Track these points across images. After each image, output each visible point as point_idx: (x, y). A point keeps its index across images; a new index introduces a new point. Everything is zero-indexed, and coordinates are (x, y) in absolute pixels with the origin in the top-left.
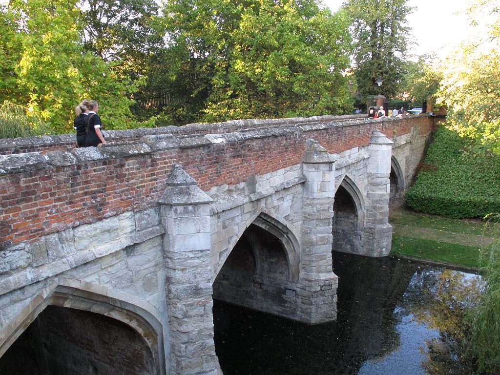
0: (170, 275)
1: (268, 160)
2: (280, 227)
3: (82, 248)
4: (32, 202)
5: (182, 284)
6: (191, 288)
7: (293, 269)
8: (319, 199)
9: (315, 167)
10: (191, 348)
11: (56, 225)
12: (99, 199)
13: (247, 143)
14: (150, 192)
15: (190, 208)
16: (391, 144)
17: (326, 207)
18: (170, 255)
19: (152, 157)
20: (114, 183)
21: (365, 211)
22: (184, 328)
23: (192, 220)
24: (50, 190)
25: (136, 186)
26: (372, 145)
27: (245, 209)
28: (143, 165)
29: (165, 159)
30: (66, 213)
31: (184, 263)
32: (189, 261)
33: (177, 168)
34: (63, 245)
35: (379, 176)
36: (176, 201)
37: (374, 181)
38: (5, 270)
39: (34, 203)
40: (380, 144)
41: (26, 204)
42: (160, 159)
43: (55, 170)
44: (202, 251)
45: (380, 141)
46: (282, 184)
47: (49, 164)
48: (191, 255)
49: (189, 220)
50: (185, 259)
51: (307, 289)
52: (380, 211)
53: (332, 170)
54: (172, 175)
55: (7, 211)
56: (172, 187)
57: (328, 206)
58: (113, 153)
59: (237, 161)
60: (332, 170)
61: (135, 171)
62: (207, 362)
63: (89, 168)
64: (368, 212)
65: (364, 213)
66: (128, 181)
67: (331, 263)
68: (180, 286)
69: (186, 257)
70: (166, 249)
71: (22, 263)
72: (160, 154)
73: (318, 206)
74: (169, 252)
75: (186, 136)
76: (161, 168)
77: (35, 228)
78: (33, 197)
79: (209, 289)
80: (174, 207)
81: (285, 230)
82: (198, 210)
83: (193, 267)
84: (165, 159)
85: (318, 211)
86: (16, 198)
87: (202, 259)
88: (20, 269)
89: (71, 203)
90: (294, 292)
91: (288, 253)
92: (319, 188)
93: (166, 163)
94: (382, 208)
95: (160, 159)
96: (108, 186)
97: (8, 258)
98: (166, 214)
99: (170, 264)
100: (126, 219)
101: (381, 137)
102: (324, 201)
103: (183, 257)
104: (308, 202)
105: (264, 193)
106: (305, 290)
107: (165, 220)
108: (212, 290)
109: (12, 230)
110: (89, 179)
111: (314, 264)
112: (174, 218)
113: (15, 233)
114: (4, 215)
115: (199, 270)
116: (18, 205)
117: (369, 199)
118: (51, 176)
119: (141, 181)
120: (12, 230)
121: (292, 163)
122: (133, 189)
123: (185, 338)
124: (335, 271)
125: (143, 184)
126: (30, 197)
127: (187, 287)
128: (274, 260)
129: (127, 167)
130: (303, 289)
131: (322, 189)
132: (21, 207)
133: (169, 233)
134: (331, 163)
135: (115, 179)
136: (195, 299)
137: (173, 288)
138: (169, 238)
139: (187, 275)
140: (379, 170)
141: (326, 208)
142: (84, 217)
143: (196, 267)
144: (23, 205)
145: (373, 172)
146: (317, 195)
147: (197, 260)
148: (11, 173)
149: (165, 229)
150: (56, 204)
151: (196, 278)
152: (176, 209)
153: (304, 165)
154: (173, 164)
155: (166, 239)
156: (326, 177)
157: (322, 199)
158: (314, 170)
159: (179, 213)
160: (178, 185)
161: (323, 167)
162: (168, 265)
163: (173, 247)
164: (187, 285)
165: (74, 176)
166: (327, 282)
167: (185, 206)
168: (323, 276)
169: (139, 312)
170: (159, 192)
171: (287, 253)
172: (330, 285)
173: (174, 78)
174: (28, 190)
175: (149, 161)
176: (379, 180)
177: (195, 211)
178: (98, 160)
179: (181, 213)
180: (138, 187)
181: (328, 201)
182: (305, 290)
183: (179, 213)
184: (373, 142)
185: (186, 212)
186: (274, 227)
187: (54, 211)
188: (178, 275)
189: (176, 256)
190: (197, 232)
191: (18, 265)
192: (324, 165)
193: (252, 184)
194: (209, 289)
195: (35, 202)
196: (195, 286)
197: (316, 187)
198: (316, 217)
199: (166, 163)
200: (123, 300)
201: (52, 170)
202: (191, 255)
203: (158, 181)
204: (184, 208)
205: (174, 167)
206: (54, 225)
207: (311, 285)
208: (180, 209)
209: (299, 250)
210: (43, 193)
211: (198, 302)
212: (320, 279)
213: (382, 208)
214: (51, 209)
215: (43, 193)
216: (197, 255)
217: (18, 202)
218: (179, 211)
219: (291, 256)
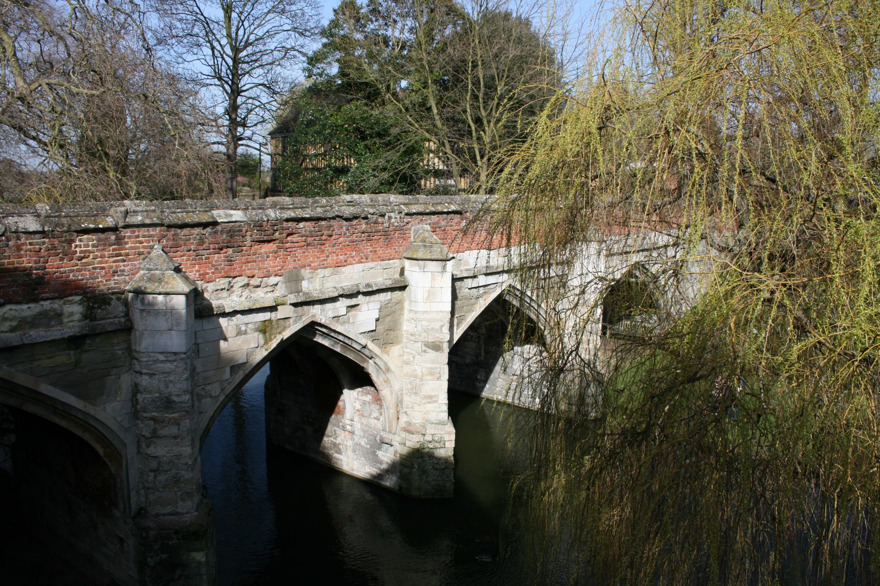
1: (328, 250)
9: (419, 266)
10: (162, 478)
14: (114, 276)
17: (437, 325)
22: (151, 451)
28: (105, 244)
29: (138, 237)
42: (129, 237)
44: (175, 354)
46: (357, 285)
48: (161, 357)
50: (154, 361)
61: (90, 248)
62: (183, 500)
63: (23, 240)
67: (445, 408)
69: (155, 359)
73: (425, 323)
74: (136, 351)
75: (179, 210)
76: (132, 248)
80: (141, 296)
83: (166, 373)
84: (138, 237)
87: (175, 364)
93: (141, 242)
95: (129, 237)
103: (152, 359)
105: (315, 295)
112: (141, 310)
115: (172, 378)
121: (379, 257)
123: (154, 464)
125: (103, 265)
129: (78, 243)
136: (167, 415)
137: (140, 397)
138: (135, 334)
143: (168, 373)
147: (168, 365)
154: (151, 243)
158: (417, 269)
163: (140, 345)
164: (157, 395)
169: (91, 422)
170: (127, 277)
180: (94, 268)
186: (346, 346)
188: (144, 381)
190: (170, 330)
193: (294, 280)
196: (166, 397)
199: (141, 242)
200: (63, 400)
202: (161, 357)
210: (439, 123)
211: (170, 419)
216: (170, 359)
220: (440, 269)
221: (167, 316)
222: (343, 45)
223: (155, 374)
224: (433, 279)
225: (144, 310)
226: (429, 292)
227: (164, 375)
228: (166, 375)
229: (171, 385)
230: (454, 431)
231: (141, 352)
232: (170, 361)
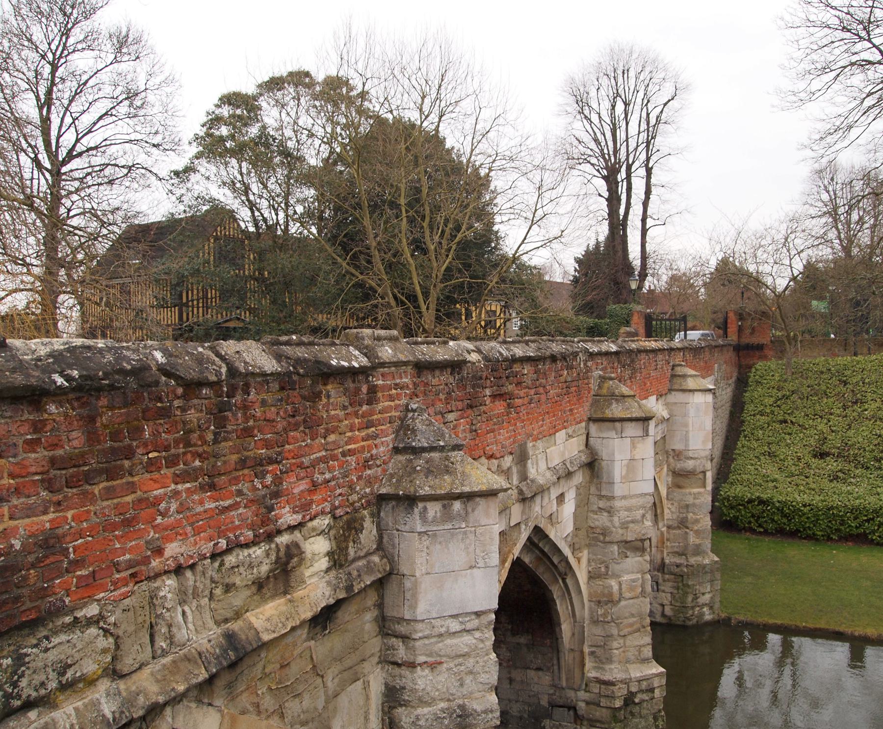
0: (398, 683)
2: (556, 560)
3: (229, 615)
4: (124, 480)
5: (429, 704)
6: (450, 712)
7: (568, 658)
8: (624, 497)
11: (178, 550)
12: (269, 479)
13: (517, 368)
15: (457, 505)
16: (710, 390)
18: (402, 629)
19: (369, 381)
20: (298, 440)
21: (664, 529)
23: (460, 537)
24: (167, 448)
25: (341, 450)
26: (673, 393)
27: (512, 517)
30: (199, 514)
31: (436, 648)
32: (449, 641)
33: (414, 411)
34: (186, 608)
35: (691, 454)
36: (427, 488)
37: (679, 465)
38: (43, 692)
39: (128, 483)
40: (690, 391)
41: (110, 483)
43: (180, 391)
45: (691, 383)
47: (168, 374)
48: (455, 626)
49: (453, 535)
51: (604, 702)
52: (696, 528)
53: (647, 435)
54: (404, 428)
55: (59, 503)
56: (408, 457)
57: (641, 512)
58: (298, 362)
59: (500, 407)
60: (647, 435)
64: (672, 531)
65: (662, 533)
66: (325, 438)
68: (426, 710)
69: (443, 630)
70: (390, 613)
71: (90, 667)
72: (383, 375)
73: (623, 514)
74: (401, 620)
77: (128, 556)
78: (127, 463)
79: (492, 711)
81: (562, 567)
82: (473, 511)
85: (623, 524)
86: (85, 464)
87: (477, 634)
88: (81, 685)
89: (212, 487)
90: (571, 713)
91: (562, 620)
92: (623, 474)
94: (697, 521)
96: (287, 446)
97: (55, 651)
98: (396, 522)
99: (402, 653)
100: (319, 535)
101: (691, 376)
102: (634, 502)
104: (602, 504)
106: (598, 705)
107: (391, 539)
108: (498, 714)
109: (70, 562)
110: (251, 423)
111: (615, 644)
112: (420, 533)
113: (79, 573)
114: (51, 516)
116: (88, 487)
117: (672, 504)
118: (170, 406)
119: (350, 438)
120: (70, 562)
122: (334, 458)
124: (658, 658)
126: (119, 463)
127: (443, 710)
128: (523, 640)
130: (594, 704)
131: (631, 473)
132: (96, 492)
133: (404, 569)
134: (645, 420)
135: (302, 428)
139: (442, 678)
140: (691, 442)
141: (639, 517)
142: (238, 527)
144: (102, 485)
145: (678, 446)
146: (619, 490)
147: (467, 639)
148: (79, 388)
149: (391, 561)
150: (180, 487)
151: (462, 685)
152: (425, 508)
153: (591, 424)
155: (391, 589)
156: (637, 450)
157: (631, 497)
159: (430, 519)
160: (423, 450)
161: (632, 430)
162: (394, 655)
163: (413, 607)
165: (219, 414)
166: (645, 683)
167: (446, 502)
168: (636, 672)
170: (379, 469)
171: (559, 620)
172: (652, 690)
173: (832, 266)
174: (116, 445)
175: (364, 389)
176: (690, 464)
177: (467, 513)
178: (272, 374)
179: (434, 521)
180: (344, 454)
181: (641, 501)
182: (598, 705)
183: (430, 519)
184: (676, 387)
185: (447, 516)
187: (174, 507)
189: (421, 631)
190: (471, 567)
191: (78, 675)
192: (633, 424)
194: (492, 711)
195: (130, 479)
196: (459, 706)
197: (618, 471)
198: (618, 538)
201: (174, 392)
202: (455, 626)
203: (378, 441)
204: (444, 506)
205: (407, 409)
206: (172, 549)
207: (613, 692)
208: (434, 509)
209: (585, 612)
212: (631, 679)
213: (697, 521)
214: (168, 502)
215: (150, 455)
216: (469, 626)
217: (88, 478)
218: (431, 514)
219: (566, 628)
220: (640, 433)
221: (468, 541)
222: (370, 174)
223: (441, 663)
224: (633, 446)
225: (425, 533)
226: (628, 466)
227: (457, 661)
228: (461, 660)
229: (468, 680)
230: (493, 638)
231: (416, 621)
232: (468, 631)
